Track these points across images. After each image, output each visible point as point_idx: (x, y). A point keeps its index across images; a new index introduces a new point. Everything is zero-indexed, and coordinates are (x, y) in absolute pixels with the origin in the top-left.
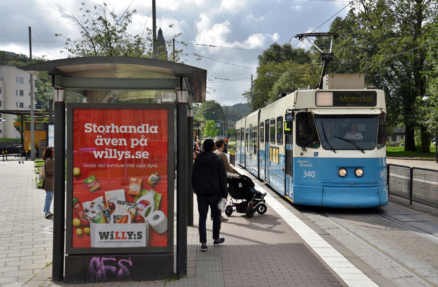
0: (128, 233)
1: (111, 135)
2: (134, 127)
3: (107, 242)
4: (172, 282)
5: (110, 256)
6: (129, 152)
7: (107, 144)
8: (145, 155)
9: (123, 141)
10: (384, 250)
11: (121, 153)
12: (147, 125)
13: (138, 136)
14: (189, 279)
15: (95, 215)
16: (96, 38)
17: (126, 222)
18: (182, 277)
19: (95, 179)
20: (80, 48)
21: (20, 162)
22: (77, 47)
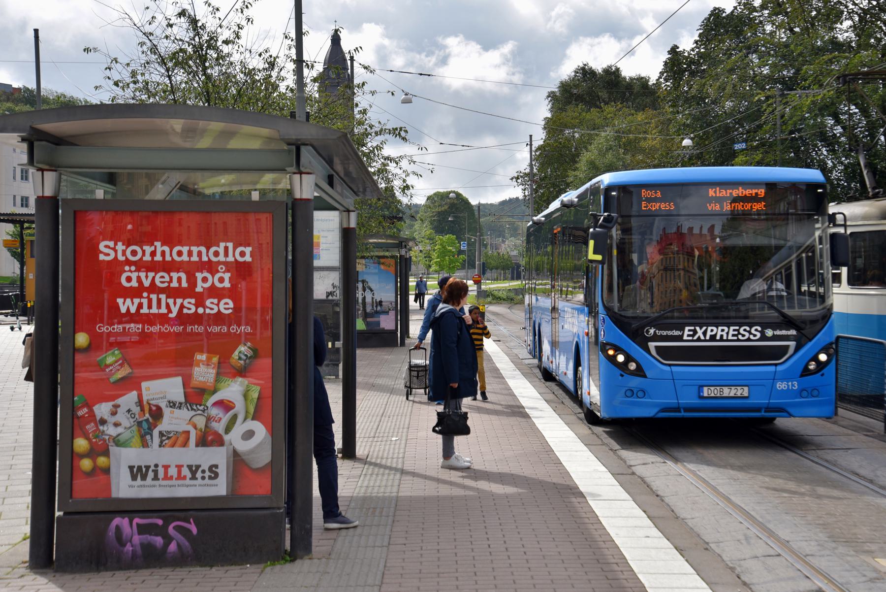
0: (190, 467)
1: (152, 267)
2: (203, 249)
3: (144, 486)
4: (278, 567)
5: (151, 514)
6: (193, 301)
7: (147, 283)
8: (226, 306)
9: (178, 279)
10: (743, 506)
11: (175, 303)
12: (230, 245)
13: (210, 267)
14: (315, 561)
15: (120, 430)
16: (174, 55)
17: (185, 444)
18: (301, 558)
19: (120, 356)
20: (139, 78)
21: (12, 329)
22: (134, 74)
